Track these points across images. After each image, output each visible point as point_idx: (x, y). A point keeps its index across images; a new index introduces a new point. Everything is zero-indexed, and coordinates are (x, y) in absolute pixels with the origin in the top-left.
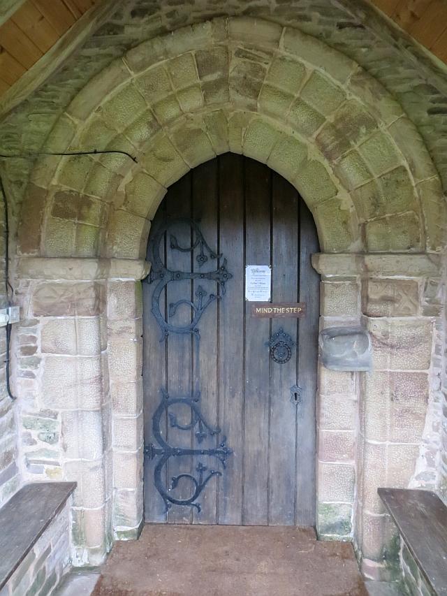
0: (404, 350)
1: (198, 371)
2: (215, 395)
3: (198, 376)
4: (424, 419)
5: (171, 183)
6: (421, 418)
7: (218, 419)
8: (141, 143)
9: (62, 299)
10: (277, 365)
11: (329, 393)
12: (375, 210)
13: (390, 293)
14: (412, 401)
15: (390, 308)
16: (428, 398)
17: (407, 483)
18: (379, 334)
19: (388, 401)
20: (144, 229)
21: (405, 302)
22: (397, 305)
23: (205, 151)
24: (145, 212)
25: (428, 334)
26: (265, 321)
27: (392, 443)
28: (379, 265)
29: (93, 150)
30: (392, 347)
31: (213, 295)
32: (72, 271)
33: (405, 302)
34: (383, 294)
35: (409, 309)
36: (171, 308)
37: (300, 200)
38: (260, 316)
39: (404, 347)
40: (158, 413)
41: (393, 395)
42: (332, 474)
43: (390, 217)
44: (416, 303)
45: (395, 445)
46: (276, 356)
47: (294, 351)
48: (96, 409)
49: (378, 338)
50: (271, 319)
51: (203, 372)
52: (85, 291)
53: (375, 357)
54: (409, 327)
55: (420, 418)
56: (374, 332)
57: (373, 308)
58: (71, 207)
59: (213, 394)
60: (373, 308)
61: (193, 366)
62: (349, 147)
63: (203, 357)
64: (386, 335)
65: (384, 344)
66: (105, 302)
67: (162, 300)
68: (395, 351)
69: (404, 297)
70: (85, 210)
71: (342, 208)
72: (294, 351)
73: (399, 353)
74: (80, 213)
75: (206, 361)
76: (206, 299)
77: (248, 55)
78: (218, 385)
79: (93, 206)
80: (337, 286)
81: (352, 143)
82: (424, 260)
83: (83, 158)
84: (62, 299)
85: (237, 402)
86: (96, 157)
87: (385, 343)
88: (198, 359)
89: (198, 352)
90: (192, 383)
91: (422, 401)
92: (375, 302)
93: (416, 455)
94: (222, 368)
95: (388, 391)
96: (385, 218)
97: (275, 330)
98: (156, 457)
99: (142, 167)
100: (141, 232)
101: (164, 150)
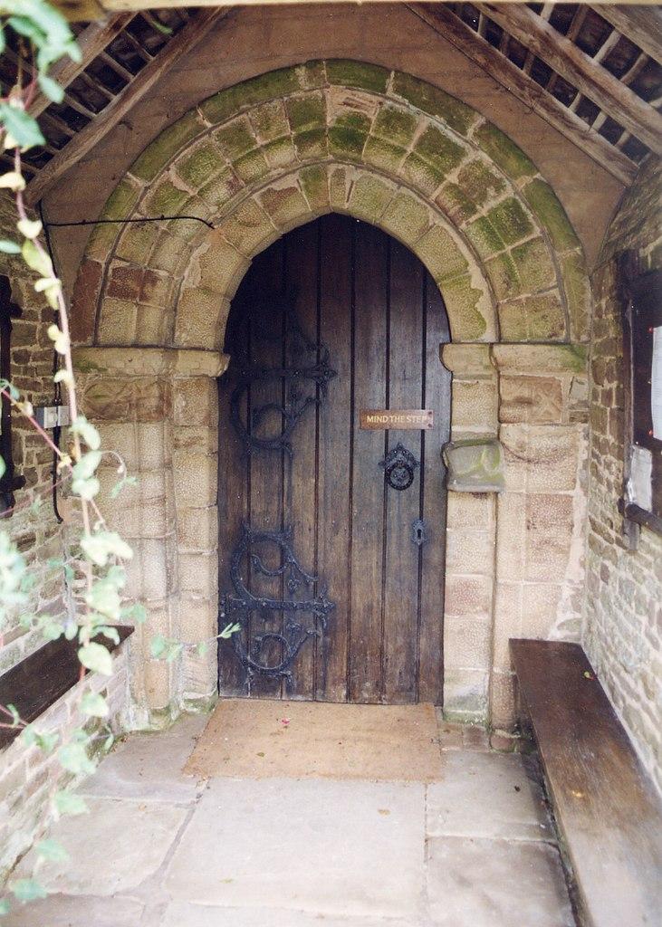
0: (543, 466)
1: (289, 498)
2: (313, 532)
3: (290, 504)
4: (568, 553)
5: (256, 252)
6: (564, 551)
7: (316, 561)
8: (219, 204)
9: (119, 398)
10: (393, 493)
11: (459, 526)
12: (507, 290)
13: (526, 393)
14: (553, 531)
15: (526, 412)
16: (573, 526)
17: (546, 633)
18: (512, 444)
19: (524, 530)
20: (221, 312)
21: (546, 405)
22: (535, 409)
23: (300, 210)
24: (222, 290)
25: (574, 446)
26: (380, 434)
27: (528, 583)
28: (511, 358)
29: (159, 216)
30: (529, 461)
31: (311, 399)
32: (132, 363)
33: (546, 405)
34: (517, 394)
35: (551, 414)
36: (257, 415)
37: (425, 271)
38: (373, 427)
39: (544, 462)
40: (241, 551)
41: (529, 522)
42: (461, 632)
43: (527, 298)
44: (559, 406)
45: (530, 586)
46: (394, 481)
47: (417, 475)
48: (159, 537)
49: (625, 498)
50: (387, 431)
51: (297, 502)
52: (146, 389)
53: (515, 478)
54: (550, 436)
55: (562, 552)
56: (506, 443)
57: (508, 412)
58: (132, 285)
59: (310, 530)
60: (508, 412)
61: (284, 494)
62: (475, 213)
63: (297, 481)
64: (522, 446)
65: (519, 458)
66: (170, 405)
67: (244, 406)
68: (532, 467)
69: (544, 397)
70: (148, 289)
71: (472, 287)
72: (417, 475)
73: (537, 469)
74: (142, 292)
75: (302, 487)
76: (301, 403)
77: (351, 102)
78: (317, 518)
79: (159, 283)
80: (468, 386)
81: (478, 207)
82: (566, 352)
83: (147, 226)
84: (119, 398)
85: (341, 539)
86: (163, 226)
87: (523, 458)
88: (290, 484)
89: (290, 474)
90: (283, 514)
91: (565, 530)
92: (509, 404)
93: (557, 597)
94: (321, 497)
95: (523, 517)
96: (520, 300)
97: (392, 445)
98: (233, 599)
99: (147, 813)
100: (217, 315)
101: (248, 212)
